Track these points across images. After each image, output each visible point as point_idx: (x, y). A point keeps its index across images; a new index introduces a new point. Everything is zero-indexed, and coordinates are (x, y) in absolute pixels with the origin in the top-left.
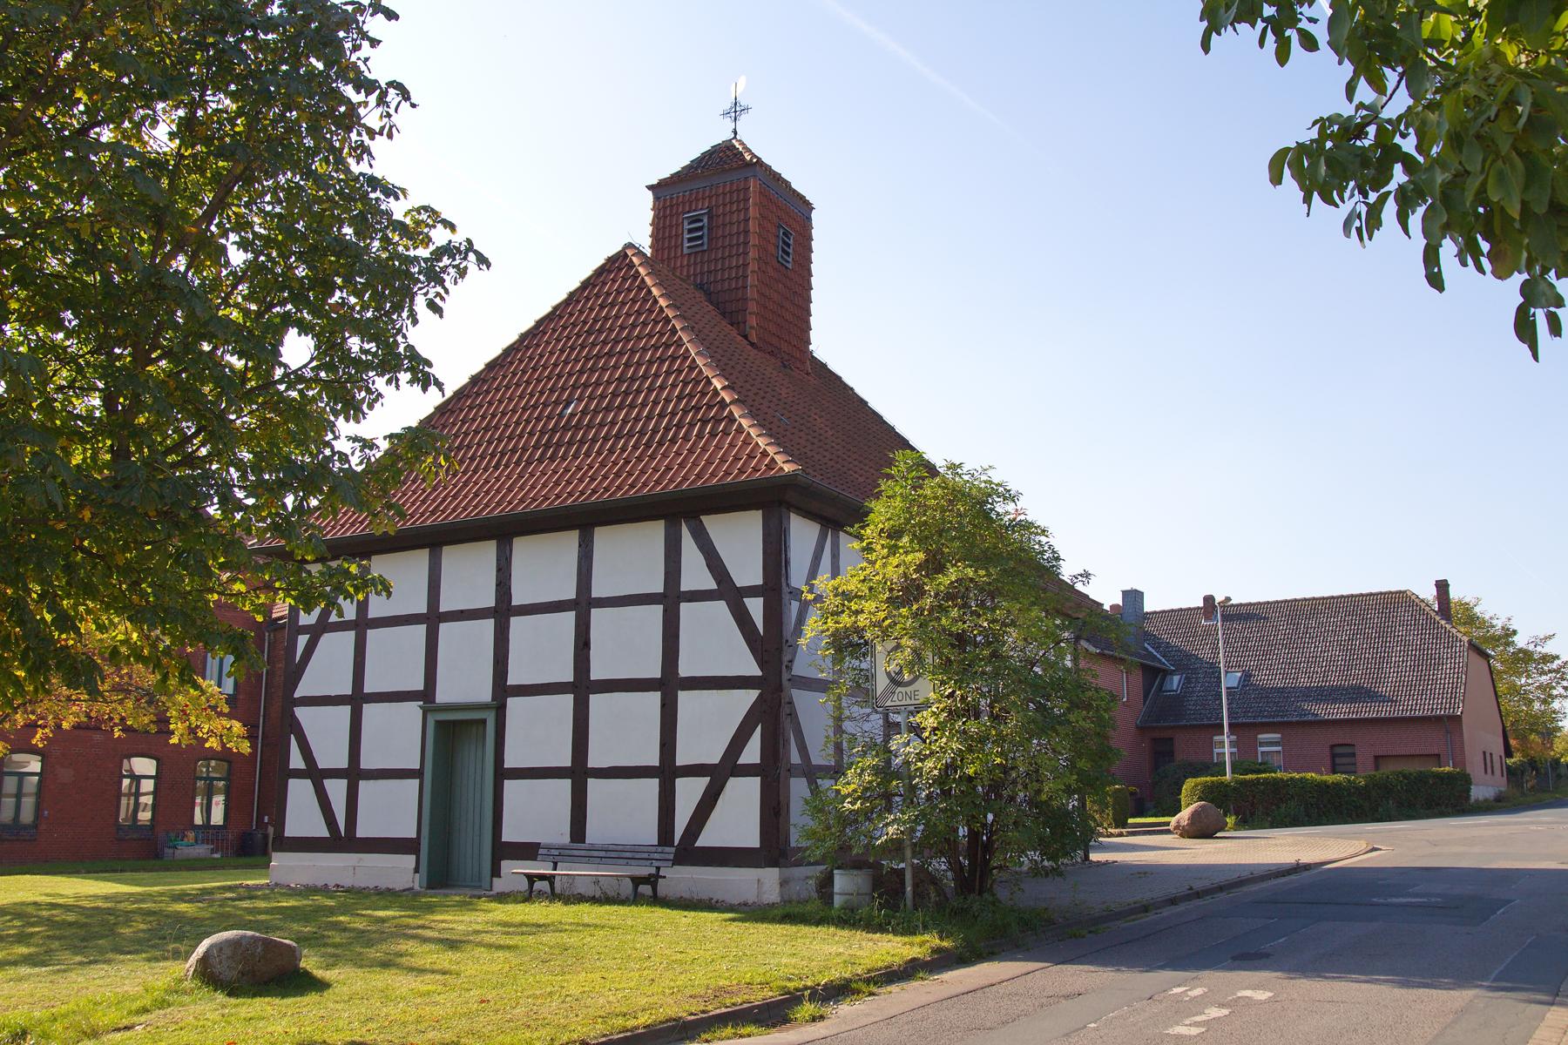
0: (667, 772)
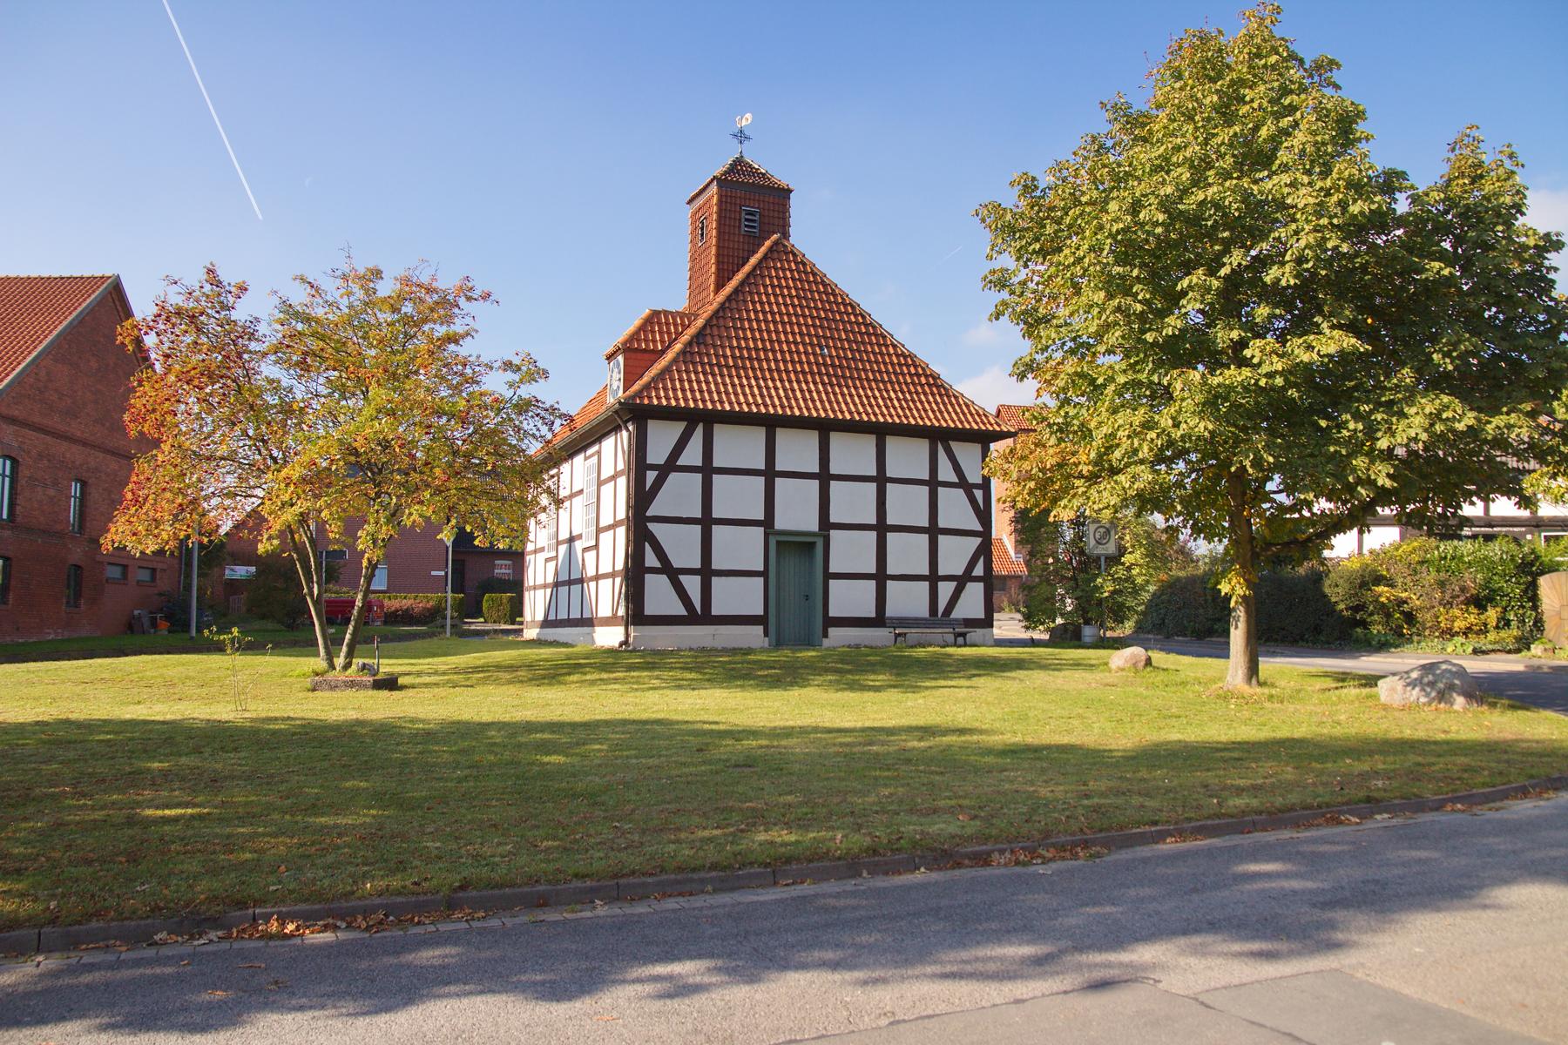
0: (933, 578)
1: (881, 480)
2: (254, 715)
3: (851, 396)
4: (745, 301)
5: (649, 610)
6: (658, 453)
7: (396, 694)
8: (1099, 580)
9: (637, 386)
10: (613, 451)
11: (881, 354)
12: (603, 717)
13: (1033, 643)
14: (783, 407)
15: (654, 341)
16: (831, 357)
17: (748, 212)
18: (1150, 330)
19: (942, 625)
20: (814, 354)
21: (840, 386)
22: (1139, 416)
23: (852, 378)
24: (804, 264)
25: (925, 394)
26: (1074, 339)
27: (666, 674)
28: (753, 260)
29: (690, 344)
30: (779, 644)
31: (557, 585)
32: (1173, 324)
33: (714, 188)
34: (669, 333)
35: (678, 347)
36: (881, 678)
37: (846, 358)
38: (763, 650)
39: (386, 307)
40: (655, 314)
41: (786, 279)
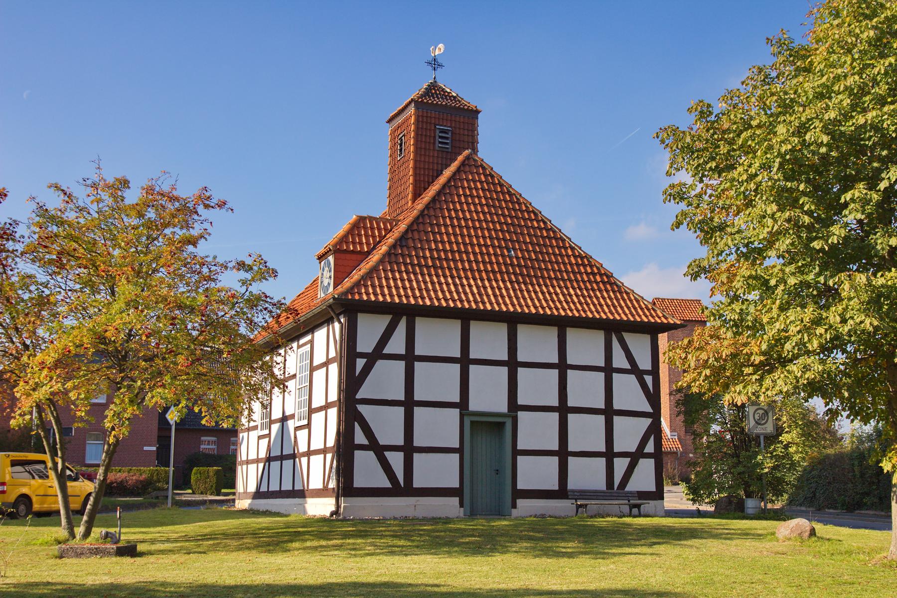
0: (610, 455)
1: (563, 367)
2: (14, 581)
3: (536, 292)
4: (441, 209)
5: (359, 482)
6: (366, 344)
7: (138, 559)
8: (760, 457)
9: (347, 283)
10: (324, 342)
11: (561, 255)
12: (334, 580)
13: (699, 514)
14: (476, 302)
15: (361, 243)
16: (517, 258)
17: (441, 130)
18: (816, 238)
19: (617, 497)
20: (503, 255)
21: (525, 284)
22: (809, 312)
23: (536, 277)
24: (492, 177)
25: (600, 291)
26: (747, 245)
27: (378, 541)
28: (447, 173)
29: (394, 246)
30: (473, 514)
31: (269, 459)
32: (837, 232)
33: (412, 110)
34: (374, 237)
35: (384, 248)
36: (571, 546)
37: (531, 259)
38: (459, 520)
39: (133, 213)
40: (361, 219)
41: (477, 189)
